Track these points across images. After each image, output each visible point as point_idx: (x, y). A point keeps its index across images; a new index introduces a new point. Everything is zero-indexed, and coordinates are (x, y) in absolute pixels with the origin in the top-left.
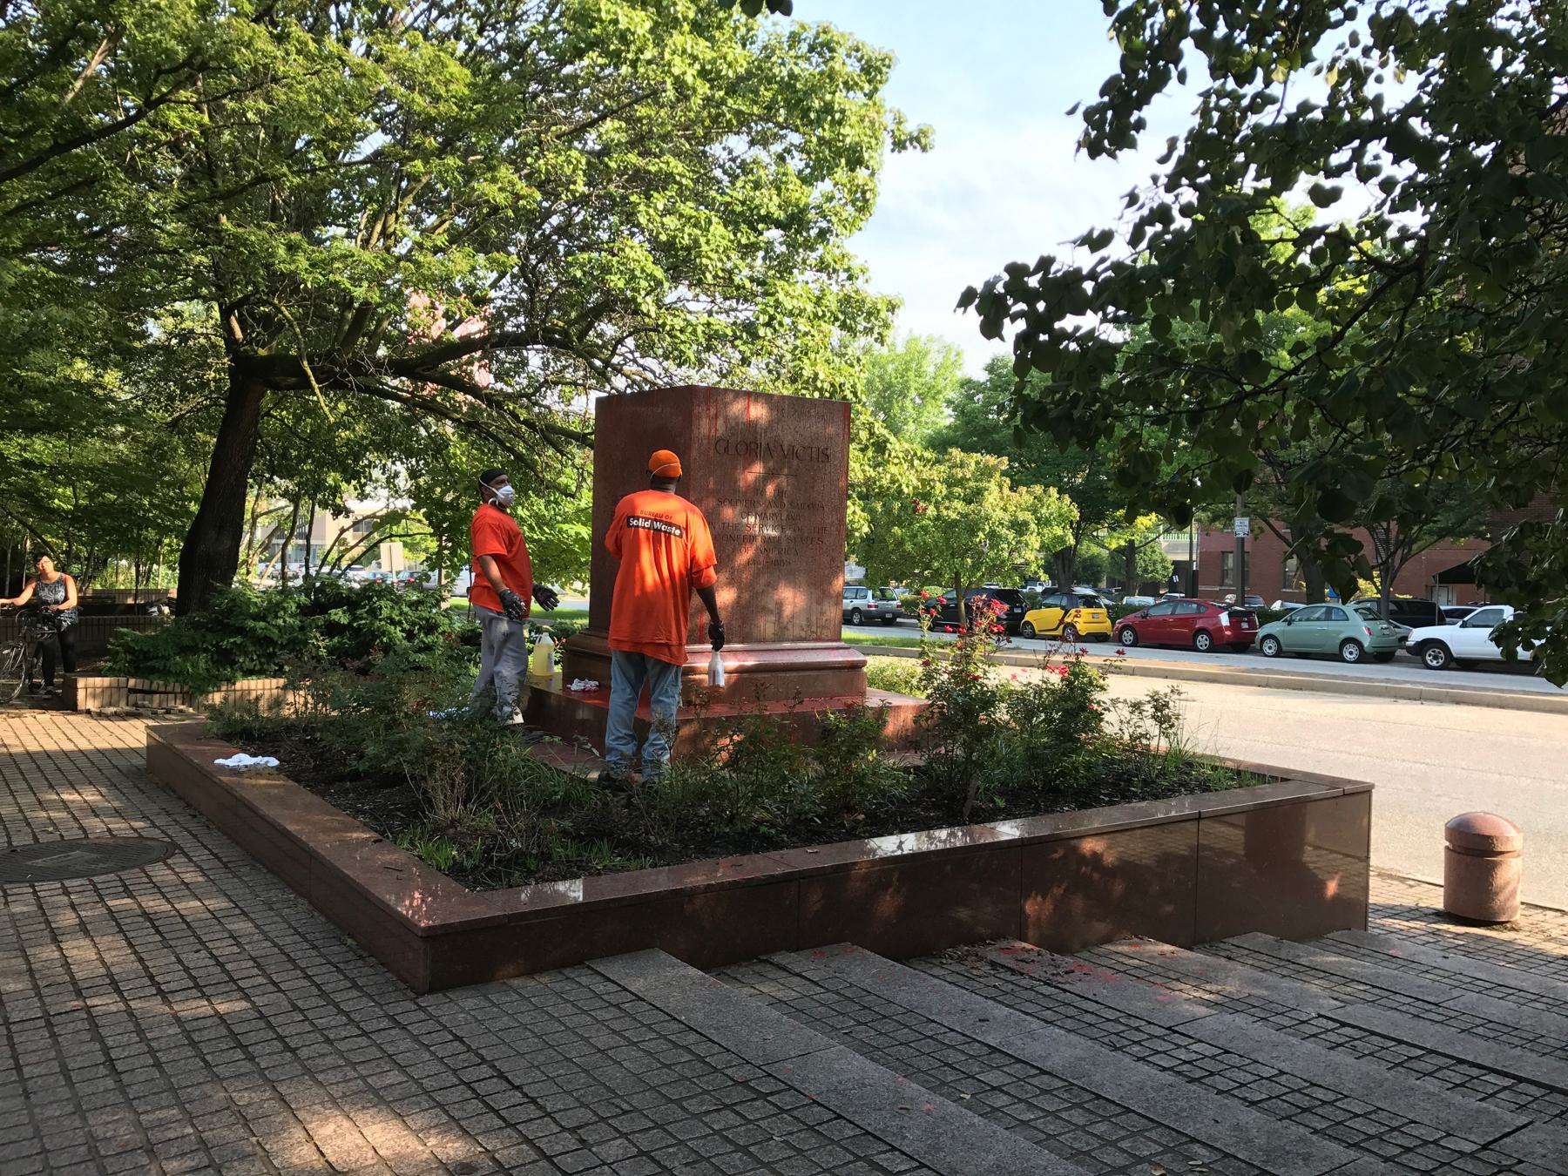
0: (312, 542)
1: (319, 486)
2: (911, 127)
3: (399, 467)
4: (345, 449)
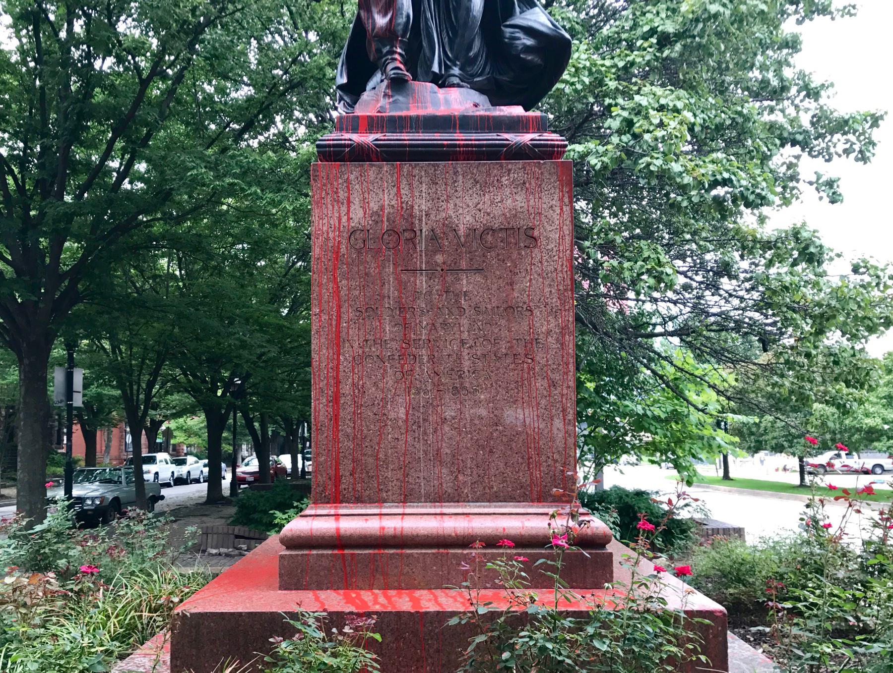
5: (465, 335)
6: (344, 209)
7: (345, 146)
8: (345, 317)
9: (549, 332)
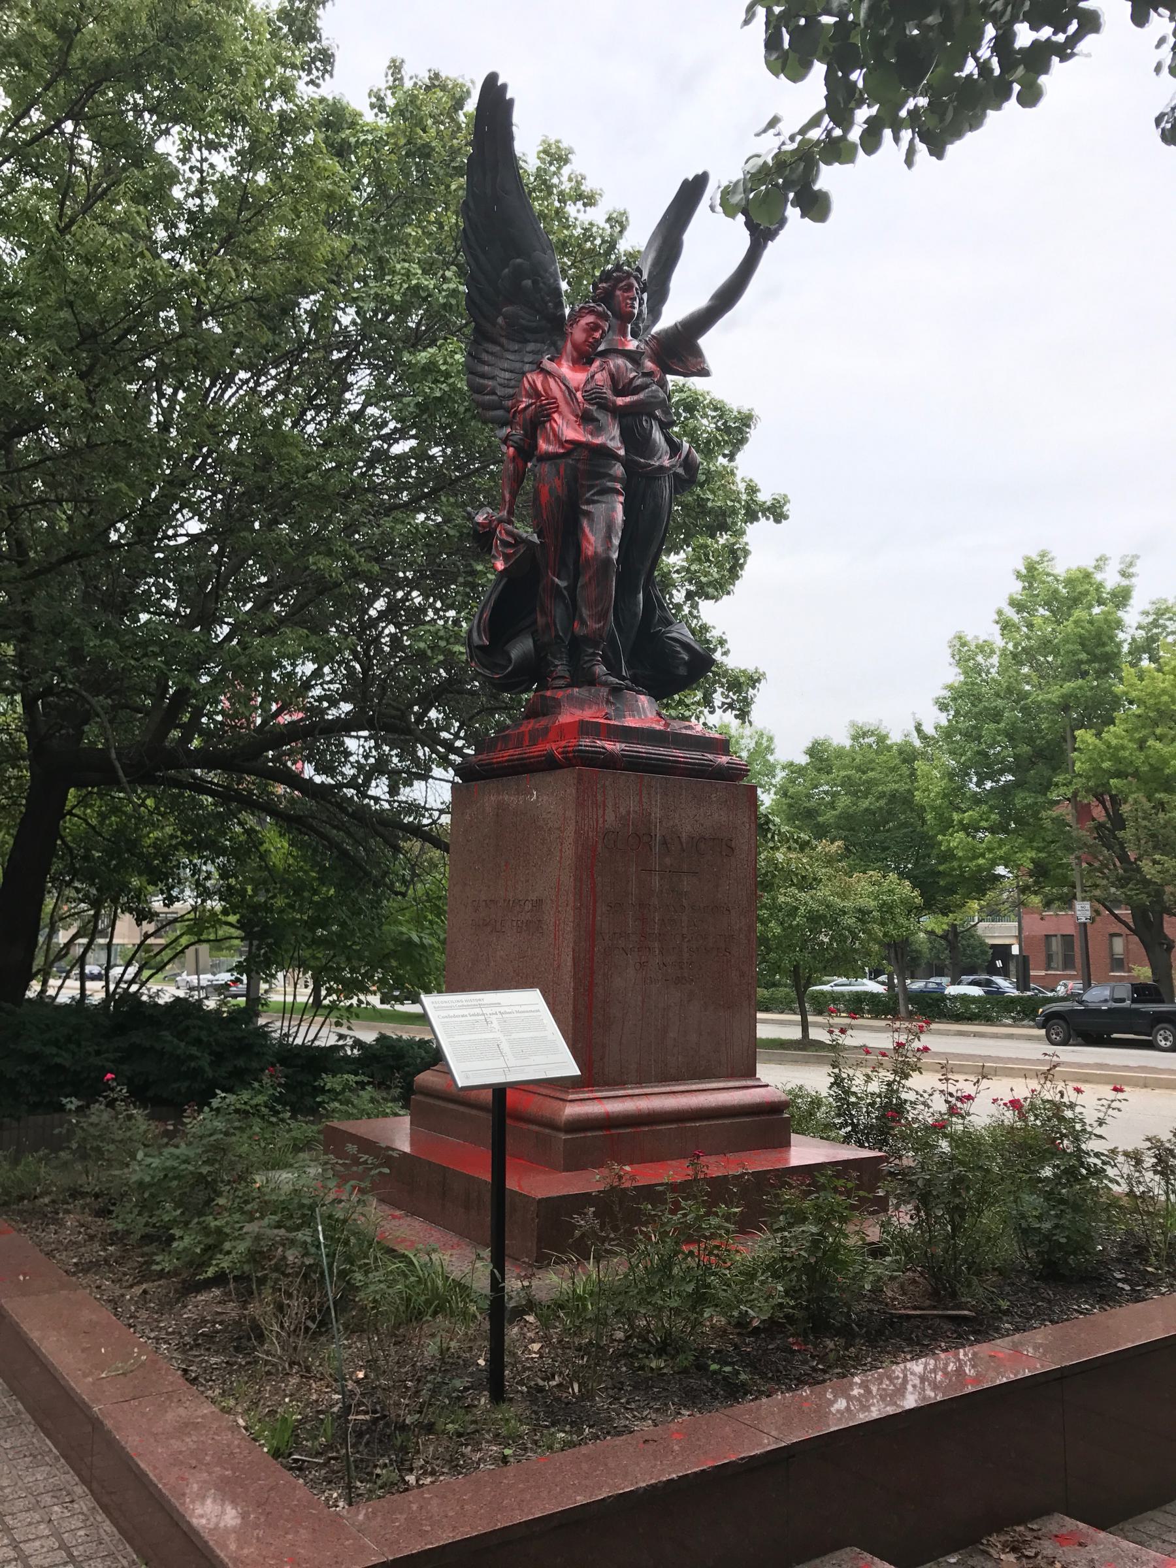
0: (115, 941)
1: (124, 887)
2: (764, 497)
3: (210, 867)
4: (151, 850)
5: (685, 931)
6: (600, 812)
7: (600, 753)
8: (599, 912)
9: (741, 929)
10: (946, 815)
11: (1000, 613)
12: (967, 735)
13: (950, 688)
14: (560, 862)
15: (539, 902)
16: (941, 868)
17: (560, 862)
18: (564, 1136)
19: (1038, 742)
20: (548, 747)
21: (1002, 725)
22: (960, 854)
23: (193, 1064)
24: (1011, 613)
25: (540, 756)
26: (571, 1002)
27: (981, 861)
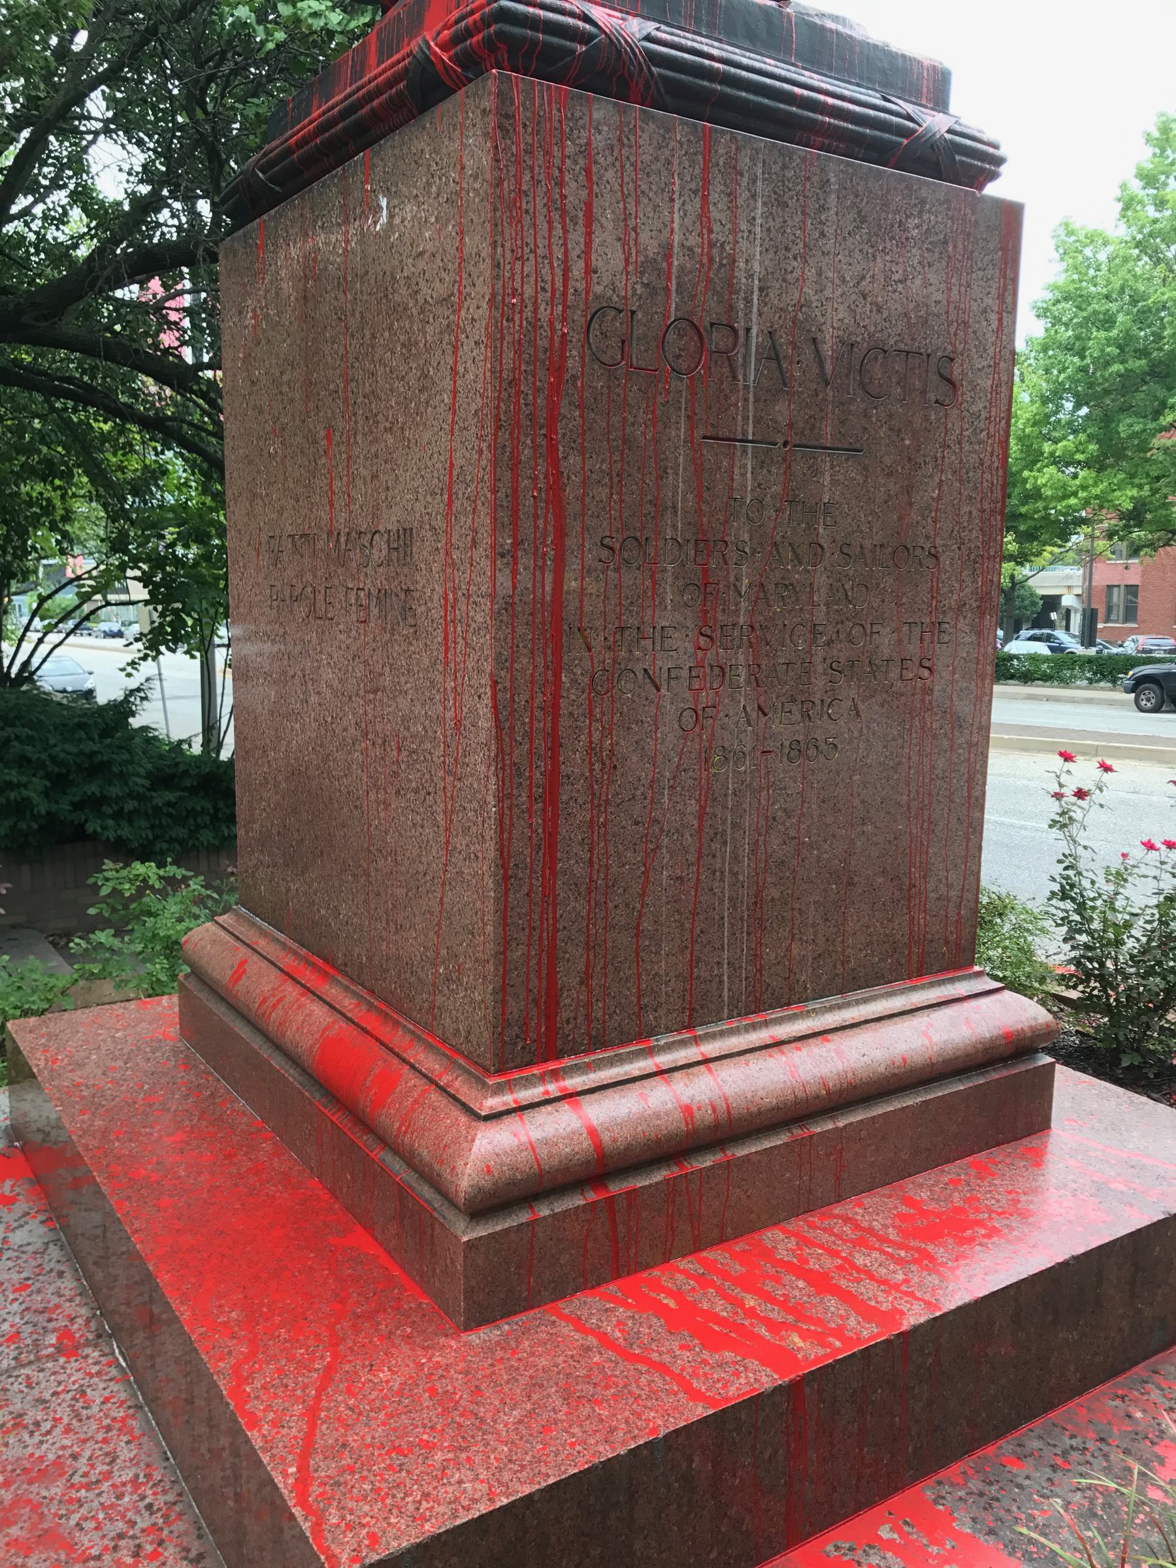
5: (820, 615)
6: (577, 237)
10: (1035, 446)
11: (1123, 187)
12: (1068, 348)
13: (1054, 288)
14: (453, 409)
15: (405, 537)
16: (1023, 510)
17: (453, 409)
18: (468, 1232)
19: (1155, 354)
20: (415, 45)
21: (1114, 333)
22: (1049, 493)
23: (13, 795)
24: (1136, 186)
25: (390, 84)
26: (490, 833)
27: (1073, 501)
